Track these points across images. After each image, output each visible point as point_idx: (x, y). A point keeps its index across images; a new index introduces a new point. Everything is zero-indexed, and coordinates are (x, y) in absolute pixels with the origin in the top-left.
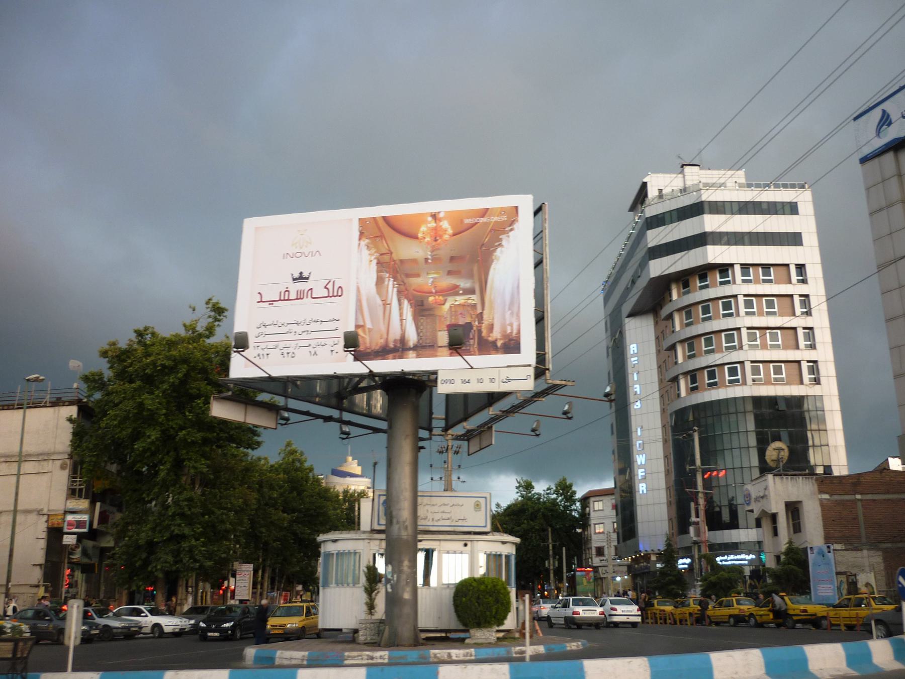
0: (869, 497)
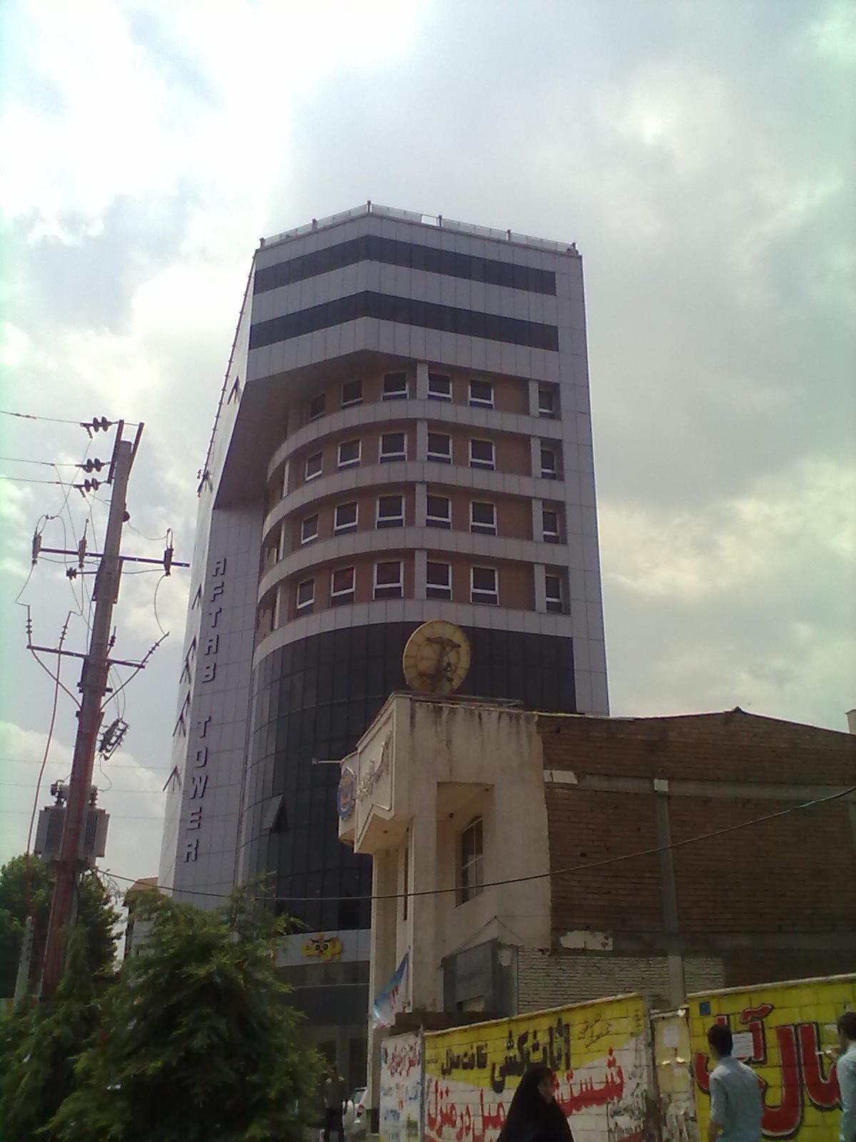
0: (692, 789)
